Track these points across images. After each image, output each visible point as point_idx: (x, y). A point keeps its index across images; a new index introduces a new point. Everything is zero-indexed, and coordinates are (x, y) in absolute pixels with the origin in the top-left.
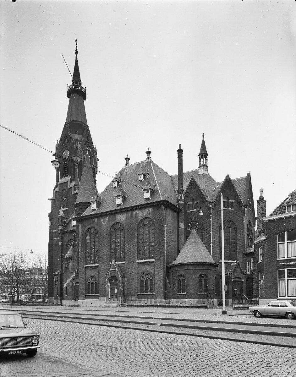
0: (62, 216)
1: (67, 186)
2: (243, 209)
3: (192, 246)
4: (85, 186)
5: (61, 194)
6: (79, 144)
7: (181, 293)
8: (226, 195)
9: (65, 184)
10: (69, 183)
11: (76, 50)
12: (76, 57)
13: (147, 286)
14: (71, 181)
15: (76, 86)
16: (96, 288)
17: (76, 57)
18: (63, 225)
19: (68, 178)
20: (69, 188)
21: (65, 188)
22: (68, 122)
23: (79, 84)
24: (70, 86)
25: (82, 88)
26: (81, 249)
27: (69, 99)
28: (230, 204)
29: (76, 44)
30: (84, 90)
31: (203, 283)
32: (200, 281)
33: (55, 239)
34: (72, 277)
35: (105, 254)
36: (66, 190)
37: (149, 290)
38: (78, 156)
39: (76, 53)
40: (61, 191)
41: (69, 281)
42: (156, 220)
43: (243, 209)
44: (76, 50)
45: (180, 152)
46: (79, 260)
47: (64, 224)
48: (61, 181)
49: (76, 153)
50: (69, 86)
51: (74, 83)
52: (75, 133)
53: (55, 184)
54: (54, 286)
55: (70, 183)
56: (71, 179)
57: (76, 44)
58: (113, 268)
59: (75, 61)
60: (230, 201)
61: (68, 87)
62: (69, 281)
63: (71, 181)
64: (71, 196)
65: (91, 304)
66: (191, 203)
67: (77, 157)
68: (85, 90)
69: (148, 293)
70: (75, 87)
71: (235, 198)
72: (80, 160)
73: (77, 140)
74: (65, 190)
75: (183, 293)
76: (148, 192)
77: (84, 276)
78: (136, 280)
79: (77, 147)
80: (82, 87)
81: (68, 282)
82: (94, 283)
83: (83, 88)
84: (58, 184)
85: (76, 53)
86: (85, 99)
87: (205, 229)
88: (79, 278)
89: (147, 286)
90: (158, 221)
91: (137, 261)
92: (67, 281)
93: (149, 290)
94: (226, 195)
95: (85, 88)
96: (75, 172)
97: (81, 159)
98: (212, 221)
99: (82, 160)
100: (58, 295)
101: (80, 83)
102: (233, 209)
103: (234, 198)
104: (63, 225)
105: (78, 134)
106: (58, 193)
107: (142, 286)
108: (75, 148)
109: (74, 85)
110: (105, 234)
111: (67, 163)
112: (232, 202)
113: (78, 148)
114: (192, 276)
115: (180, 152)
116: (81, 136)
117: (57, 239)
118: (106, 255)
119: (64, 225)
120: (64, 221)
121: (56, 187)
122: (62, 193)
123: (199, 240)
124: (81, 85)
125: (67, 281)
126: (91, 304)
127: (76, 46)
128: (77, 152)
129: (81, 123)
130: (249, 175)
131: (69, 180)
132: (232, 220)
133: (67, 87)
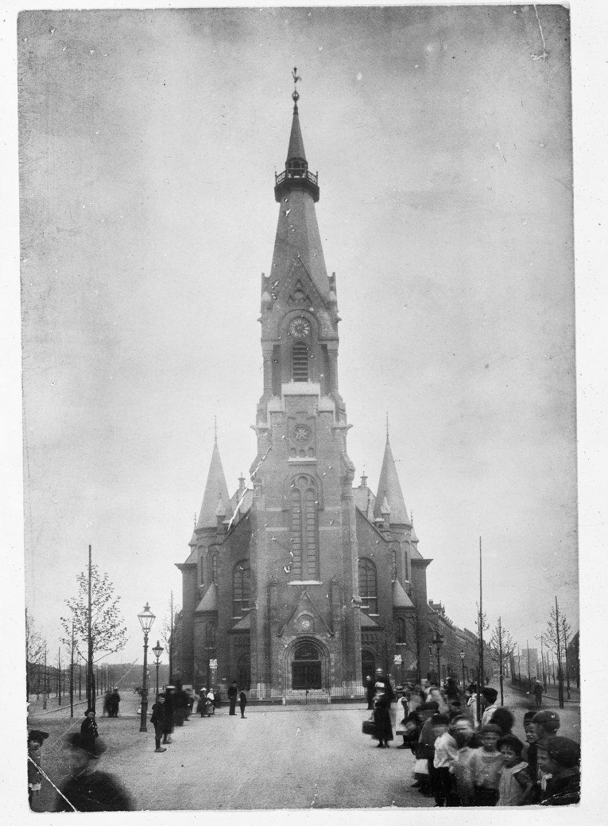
11: (296, 92)
12: (296, 108)
15: (295, 173)
17: (296, 108)
23: (303, 167)
24: (281, 174)
25: (310, 176)
27: (279, 204)
29: (296, 113)
30: (313, 178)
34: (234, 516)
45: (90, 546)
48: (527, 720)
50: (278, 175)
51: (290, 167)
57: (296, 113)
59: (290, 126)
61: (277, 177)
68: (316, 177)
70: (293, 175)
80: (308, 172)
83: (312, 174)
86: (316, 199)
95: (315, 174)
101: (305, 163)
109: (290, 172)
115: (90, 546)
124: (307, 168)
133: (274, 177)
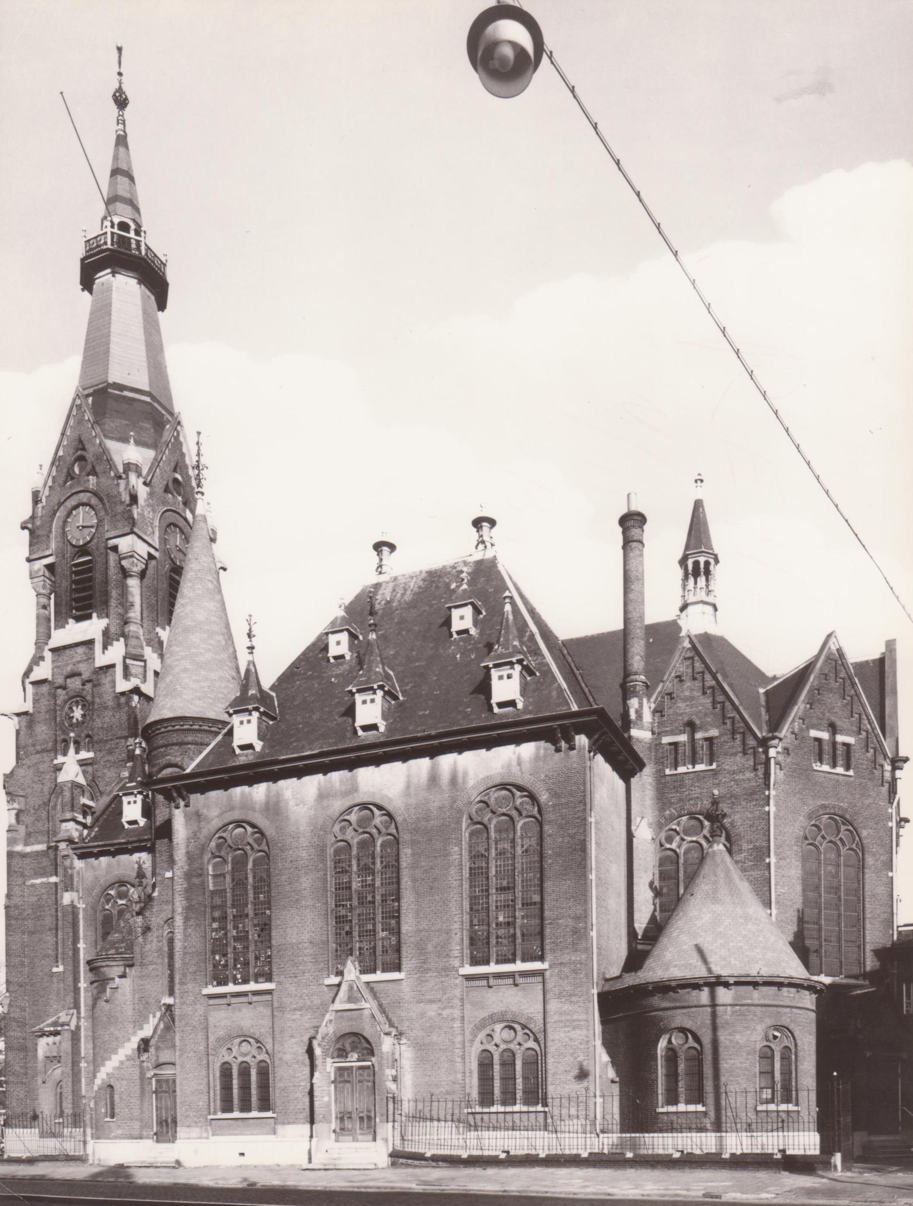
0: (73, 782)
1: (91, 658)
2: (887, 775)
3: (718, 908)
4: (194, 650)
5: (59, 691)
6: (145, 483)
7: (682, 1107)
8: (827, 714)
9: (80, 650)
10: (98, 646)
13: (245, 1088)
14: (108, 638)
16: (264, 1086)
18: (80, 818)
19: (93, 627)
20: (101, 668)
21: (84, 668)
22: (91, 391)
26: (186, 919)
28: (840, 750)
31: (777, 1065)
32: (767, 1056)
33: (38, 881)
35: (306, 937)
36: (86, 676)
37: (519, 1094)
38: (139, 537)
39: (121, 101)
40: (60, 681)
41: (123, 1058)
42: (555, 795)
43: (887, 775)
44: (120, 90)
46: (178, 964)
47: (85, 818)
48: (60, 637)
49: (133, 522)
52: (125, 440)
53: (31, 651)
54: (40, 1081)
55: (105, 647)
56: (106, 633)
58: (350, 999)
60: (840, 738)
62: (123, 1058)
63: (108, 638)
64: (110, 703)
65: (242, 1154)
66: (683, 738)
67: (135, 537)
69: (517, 1108)
71: (860, 729)
72: (149, 554)
73: (128, 467)
74: (79, 674)
75: (691, 1108)
76: (509, 677)
77: (200, 1036)
78: (458, 1052)
79: (134, 499)
81: (117, 1064)
82: (253, 1063)
84: (47, 648)
85: (121, 101)
87: (745, 846)
88: (178, 1043)
89: (245, 1088)
90: (563, 800)
91: (463, 971)
92: (113, 1057)
93: (519, 1094)
94: (827, 714)
96: (125, 605)
97: (152, 551)
98: (775, 813)
99: (156, 554)
100: (61, 1115)
102: (851, 773)
103: (855, 729)
104: (80, 818)
105: (138, 443)
106: (45, 689)
107: (227, 1087)
108: (126, 498)
110: (304, 854)
111: (89, 562)
112: (847, 745)
113: (141, 500)
114: (731, 1034)
116: (151, 454)
117: (42, 883)
118: (311, 942)
119: (84, 821)
120: (84, 805)
121: (37, 659)
122: (64, 688)
123: (745, 887)
125: (113, 1057)
126: (242, 1154)
127: (120, 74)
128: (133, 519)
129: (148, 399)
130: (891, 646)
131: (101, 634)
132: (848, 817)
